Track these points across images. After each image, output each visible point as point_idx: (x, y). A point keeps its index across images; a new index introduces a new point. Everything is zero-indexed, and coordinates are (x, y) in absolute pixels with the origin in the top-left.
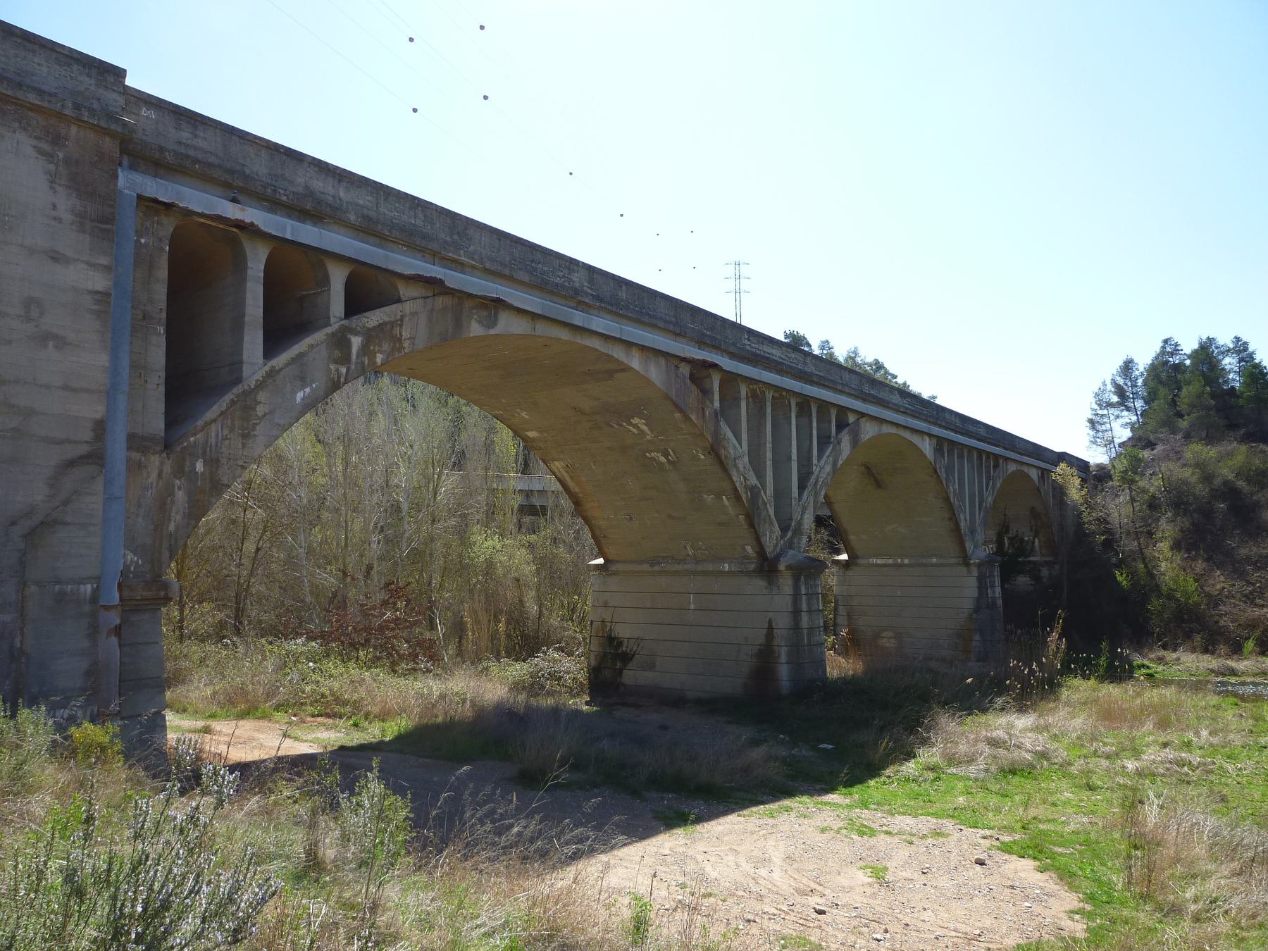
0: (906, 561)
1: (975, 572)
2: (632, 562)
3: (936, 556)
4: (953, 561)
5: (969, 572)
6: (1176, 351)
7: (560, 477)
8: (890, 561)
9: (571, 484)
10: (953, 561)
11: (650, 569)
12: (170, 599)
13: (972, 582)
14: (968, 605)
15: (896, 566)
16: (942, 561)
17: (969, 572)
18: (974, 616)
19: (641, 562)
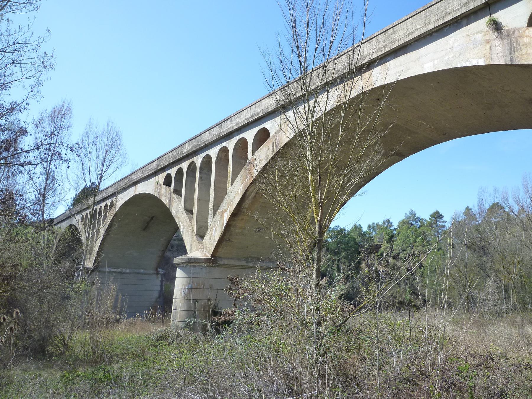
0: (128, 271)
1: (160, 278)
2: (233, 259)
3: (142, 269)
4: (151, 272)
5: (157, 278)
6: (391, 225)
7: (247, 194)
8: (119, 270)
9: (248, 201)
10: (151, 272)
11: (246, 265)
12: (71, 226)
13: (158, 283)
14: (156, 294)
15: (122, 273)
16: (146, 272)
17: (157, 278)
18: (158, 299)
19: (239, 259)
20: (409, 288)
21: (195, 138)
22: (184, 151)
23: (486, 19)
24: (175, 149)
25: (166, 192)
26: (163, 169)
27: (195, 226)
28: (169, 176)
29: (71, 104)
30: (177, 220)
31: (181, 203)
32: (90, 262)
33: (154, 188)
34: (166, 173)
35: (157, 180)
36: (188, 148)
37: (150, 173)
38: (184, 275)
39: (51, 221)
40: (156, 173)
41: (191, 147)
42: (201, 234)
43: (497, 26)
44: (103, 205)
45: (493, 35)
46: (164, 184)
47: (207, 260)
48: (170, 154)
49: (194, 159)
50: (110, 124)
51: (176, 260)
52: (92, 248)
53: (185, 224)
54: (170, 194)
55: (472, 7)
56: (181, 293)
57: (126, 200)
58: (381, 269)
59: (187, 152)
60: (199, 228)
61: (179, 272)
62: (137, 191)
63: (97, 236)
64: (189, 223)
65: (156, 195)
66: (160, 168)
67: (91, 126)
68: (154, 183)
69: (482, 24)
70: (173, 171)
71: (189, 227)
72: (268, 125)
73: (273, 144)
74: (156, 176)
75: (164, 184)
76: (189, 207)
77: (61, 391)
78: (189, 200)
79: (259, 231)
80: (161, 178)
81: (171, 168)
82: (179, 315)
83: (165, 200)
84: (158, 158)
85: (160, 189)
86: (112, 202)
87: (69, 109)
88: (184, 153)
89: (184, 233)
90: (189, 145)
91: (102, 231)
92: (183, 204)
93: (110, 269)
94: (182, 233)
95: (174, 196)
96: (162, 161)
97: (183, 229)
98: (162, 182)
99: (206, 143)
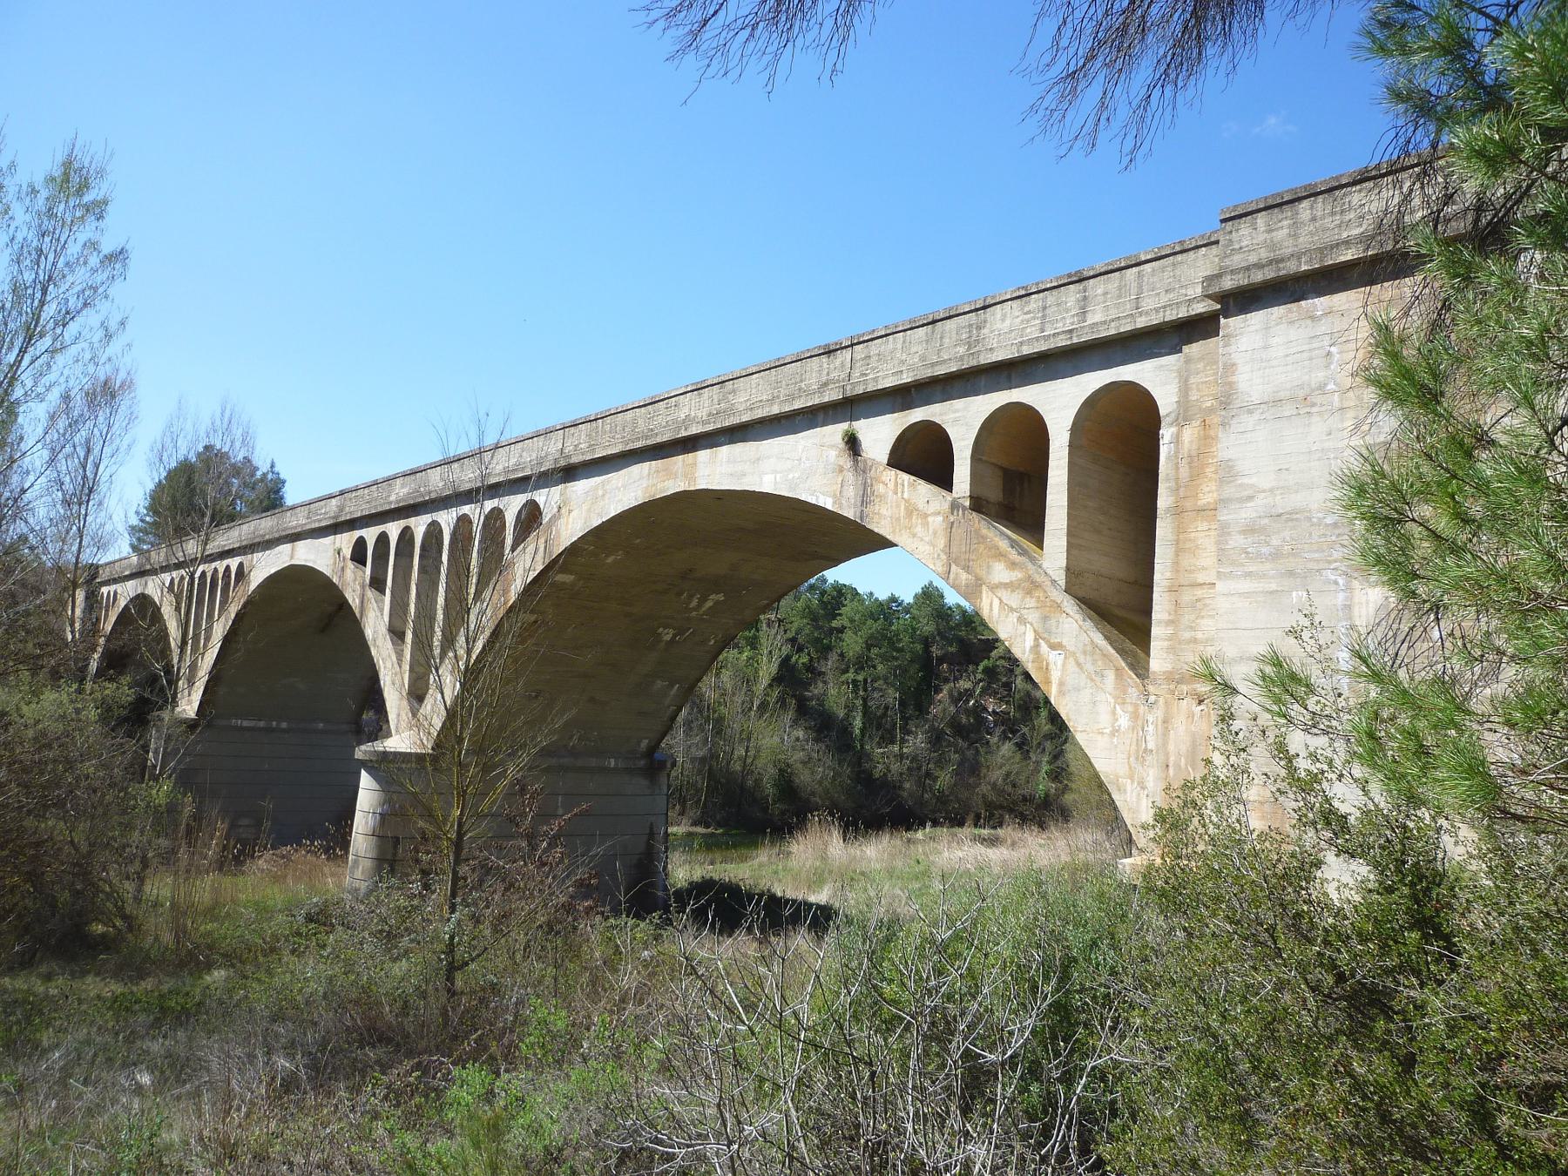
0: (284, 725)
8: (262, 724)
20: (1050, 763)
21: (414, 472)
22: (393, 498)
23: (844, 426)
24: (376, 483)
25: (355, 580)
26: (351, 524)
27: (407, 675)
28: (361, 543)
29: (132, 372)
30: (374, 652)
31: (382, 615)
32: (190, 702)
33: (332, 561)
34: (357, 534)
35: (337, 545)
36: (400, 493)
37: (323, 524)
38: (374, 785)
39: (94, 569)
40: (336, 528)
41: (405, 490)
42: (417, 695)
43: (852, 443)
44: (221, 566)
45: (846, 462)
46: (352, 559)
47: (420, 758)
48: (366, 491)
49: (412, 522)
50: (228, 407)
51: (362, 751)
52: (193, 667)
53: (389, 665)
54: (363, 587)
55: (826, 399)
56: (367, 823)
57: (273, 571)
58: (991, 704)
59: (398, 501)
60: (416, 681)
61: (365, 780)
62: (296, 557)
63: (207, 639)
64: (396, 666)
65: (335, 580)
66: (343, 519)
67: (181, 420)
68: (331, 553)
69: (834, 433)
70: (370, 534)
71: (396, 674)
72: (540, 496)
73: (546, 542)
74: (335, 534)
75: (352, 559)
76: (398, 624)
77: (110, 1024)
78: (399, 608)
79: (536, 696)
80: (346, 541)
81: (367, 526)
82: (361, 868)
83: (353, 598)
84: (342, 493)
85: (343, 568)
86: (241, 565)
87: (127, 385)
88: (391, 503)
89: (387, 683)
90: (403, 486)
91: (219, 630)
92: (386, 619)
93: (239, 721)
94: (382, 682)
95: (370, 593)
96: (348, 503)
97: (384, 676)
98: (347, 552)
99: (433, 496)
